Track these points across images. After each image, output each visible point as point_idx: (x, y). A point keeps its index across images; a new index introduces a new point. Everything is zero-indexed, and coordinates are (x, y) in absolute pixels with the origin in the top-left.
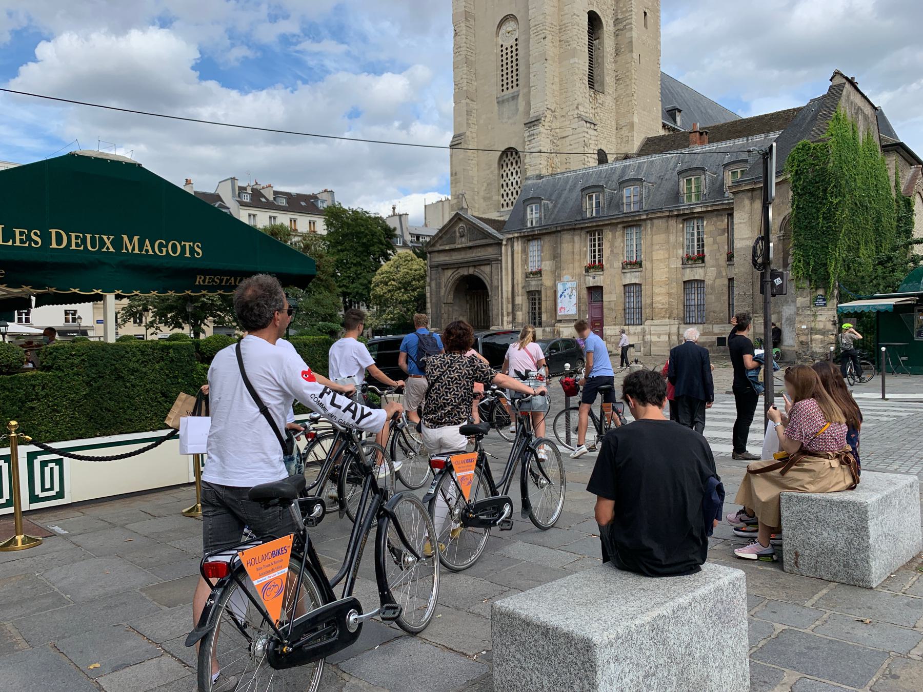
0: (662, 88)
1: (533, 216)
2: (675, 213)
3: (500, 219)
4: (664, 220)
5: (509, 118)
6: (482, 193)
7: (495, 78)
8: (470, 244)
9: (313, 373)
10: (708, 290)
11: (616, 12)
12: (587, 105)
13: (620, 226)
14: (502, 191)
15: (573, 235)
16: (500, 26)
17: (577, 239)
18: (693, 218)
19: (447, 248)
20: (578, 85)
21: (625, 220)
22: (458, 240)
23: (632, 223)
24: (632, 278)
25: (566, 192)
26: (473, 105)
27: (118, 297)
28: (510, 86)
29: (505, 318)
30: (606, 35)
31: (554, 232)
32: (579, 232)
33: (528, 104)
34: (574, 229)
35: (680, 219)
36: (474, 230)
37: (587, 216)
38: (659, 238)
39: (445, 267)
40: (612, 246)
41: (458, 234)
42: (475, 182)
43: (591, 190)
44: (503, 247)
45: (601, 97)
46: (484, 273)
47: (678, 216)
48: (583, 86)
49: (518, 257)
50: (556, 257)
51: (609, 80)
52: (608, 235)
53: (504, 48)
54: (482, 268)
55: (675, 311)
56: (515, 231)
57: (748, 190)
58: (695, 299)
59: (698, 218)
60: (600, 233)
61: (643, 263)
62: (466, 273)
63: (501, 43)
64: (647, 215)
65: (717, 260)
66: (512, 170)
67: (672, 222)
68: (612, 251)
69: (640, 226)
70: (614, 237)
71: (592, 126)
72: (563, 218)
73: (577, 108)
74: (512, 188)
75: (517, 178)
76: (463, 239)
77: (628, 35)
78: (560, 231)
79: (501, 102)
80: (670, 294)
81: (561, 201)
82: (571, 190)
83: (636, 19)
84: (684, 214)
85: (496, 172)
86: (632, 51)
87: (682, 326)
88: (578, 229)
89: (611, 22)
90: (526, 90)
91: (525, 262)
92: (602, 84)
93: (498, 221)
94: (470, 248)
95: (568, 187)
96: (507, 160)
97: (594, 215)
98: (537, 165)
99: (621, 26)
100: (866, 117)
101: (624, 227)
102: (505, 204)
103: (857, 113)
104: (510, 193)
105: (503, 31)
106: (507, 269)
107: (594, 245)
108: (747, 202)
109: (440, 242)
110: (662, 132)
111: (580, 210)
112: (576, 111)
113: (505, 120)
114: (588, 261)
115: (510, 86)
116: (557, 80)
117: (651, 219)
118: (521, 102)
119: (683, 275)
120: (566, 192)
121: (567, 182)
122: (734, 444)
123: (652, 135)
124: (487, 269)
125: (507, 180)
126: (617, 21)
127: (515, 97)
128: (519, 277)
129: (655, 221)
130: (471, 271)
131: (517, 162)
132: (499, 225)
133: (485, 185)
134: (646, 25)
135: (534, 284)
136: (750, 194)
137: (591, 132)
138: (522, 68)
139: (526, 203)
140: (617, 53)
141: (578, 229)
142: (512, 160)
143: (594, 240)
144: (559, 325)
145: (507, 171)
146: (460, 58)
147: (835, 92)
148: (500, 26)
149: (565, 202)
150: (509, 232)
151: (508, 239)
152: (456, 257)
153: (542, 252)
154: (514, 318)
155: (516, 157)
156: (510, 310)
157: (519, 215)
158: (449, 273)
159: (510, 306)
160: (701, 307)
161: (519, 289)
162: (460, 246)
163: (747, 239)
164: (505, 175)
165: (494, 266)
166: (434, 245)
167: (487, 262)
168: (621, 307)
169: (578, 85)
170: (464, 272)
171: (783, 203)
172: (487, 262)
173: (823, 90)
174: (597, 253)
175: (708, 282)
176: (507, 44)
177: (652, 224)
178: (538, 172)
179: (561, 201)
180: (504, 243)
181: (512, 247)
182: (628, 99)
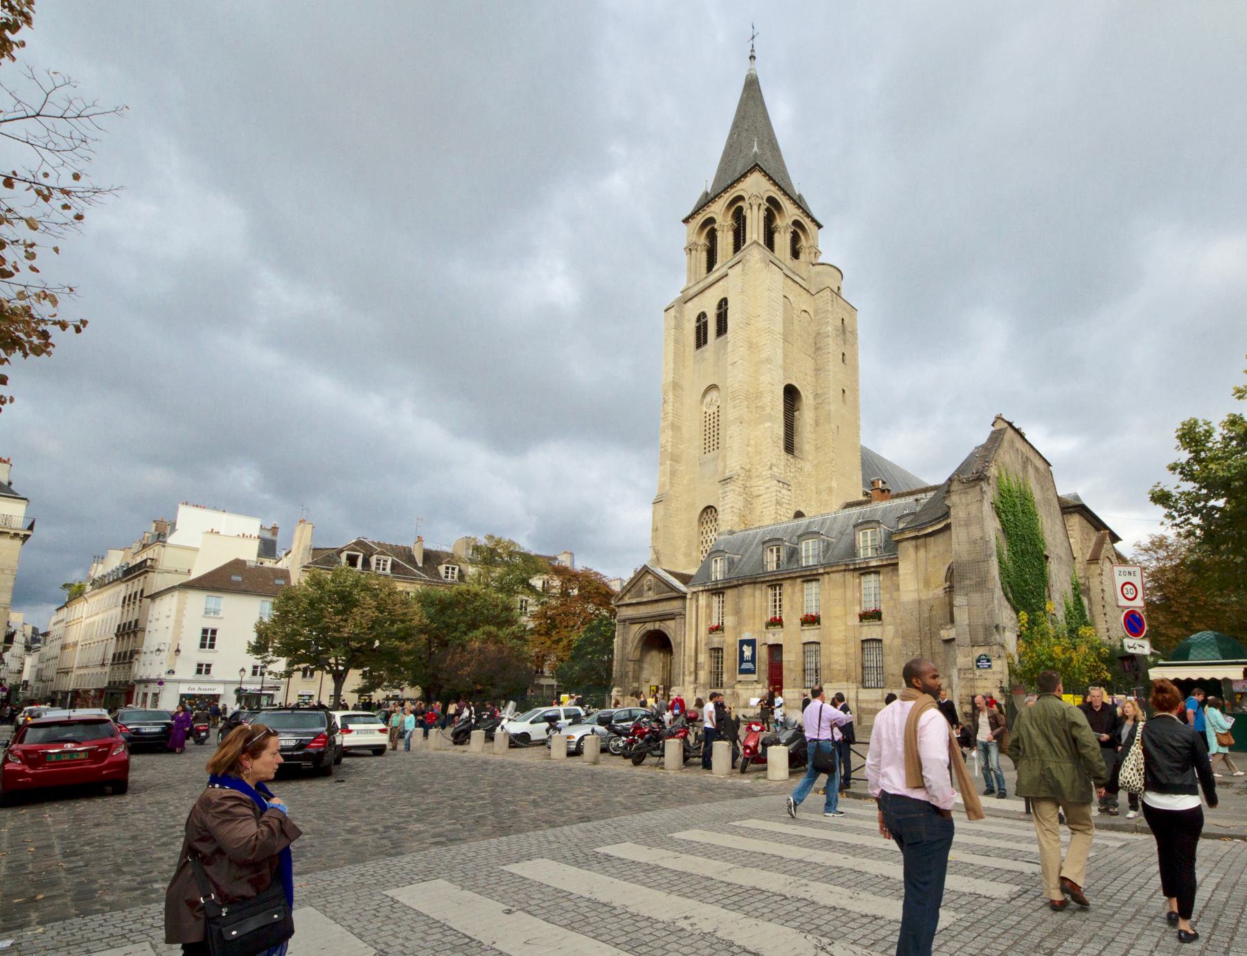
0: (862, 459)
1: (718, 570)
7: (699, 441)
8: (656, 597)
10: (886, 650)
13: (799, 580)
17: (758, 593)
18: (870, 573)
22: (645, 595)
23: (810, 577)
24: (810, 634)
27: (285, 574)
29: (687, 678)
31: (735, 586)
34: (755, 583)
35: (856, 574)
37: (771, 568)
38: (838, 593)
39: (634, 621)
40: (791, 601)
45: (801, 464)
46: (669, 628)
47: (855, 570)
49: (702, 612)
50: (737, 612)
52: (786, 584)
55: (853, 674)
56: (700, 585)
58: (872, 659)
60: (781, 585)
65: (894, 617)
67: (849, 576)
68: (791, 607)
72: (747, 570)
80: (847, 654)
81: (747, 555)
83: (833, 393)
84: (860, 569)
87: (861, 690)
89: (811, 397)
91: (710, 617)
92: (801, 451)
98: (727, 519)
99: (819, 400)
100: (1037, 469)
103: (1025, 468)
105: (708, 398)
111: (762, 564)
114: (770, 616)
117: (828, 573)
119: (861, 633)
121: (755, 538)
122: (946, 861)
124: (671, 623)
126: (816, 396)
128: (703, 630)
130: (657, 626)
132: (685, 579)
135: (716, 640)
136: (914, 542)
137: (784, 491)
140: (817, 424)
144: (738, 686)
147: (996, 438)
149: (751, 557)
150: (694, 586)
154: (696, 679)
156: (692, 669)
157: (705, 568)
158: (636, 628)
159: (693, 665)
160: (880, 669)
161: (703, 648)
167: (671, 617)
168: (800, 668)
170: (650, 626)
172: (671, 617)
173: (982, 438)
175: (885, 642)
176: (710, 411)
179: (747, 555)
180: (689, 596)
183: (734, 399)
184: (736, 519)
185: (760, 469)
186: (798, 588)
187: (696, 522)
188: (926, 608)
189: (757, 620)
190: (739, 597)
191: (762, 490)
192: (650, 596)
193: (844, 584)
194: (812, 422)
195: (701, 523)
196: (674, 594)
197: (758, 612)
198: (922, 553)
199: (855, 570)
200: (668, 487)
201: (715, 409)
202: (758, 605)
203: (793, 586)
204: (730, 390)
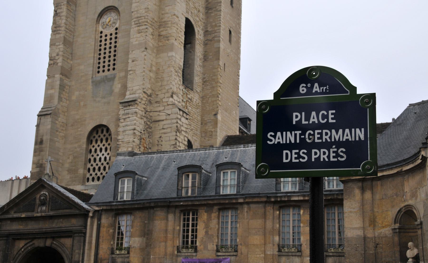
2: (273, 200)
3: (85, 192)
4: (261, 205)
5: (104, 98)
6: (67, 166)
8: (51, 213)
9: (123, 249)
11: (206, 26)
12: (180, 96)
13: (216, 208)
14: (89, 166)
15: (168, 213)
16: (101, 15)
17: (171, 217)
18: (289, 206)
19: (23, 216)
20: (174, 77)
21: (222, 202)
23: (227, 205)
25: (160, 170)
26: (66, 81)
28: (106, 68)
30: (197, 42)
32: (173, 209)
33: (125, 87)
35: (277, 207)
36: (58, 200)
38: (257, 223)
40: (207, 227)
41: (38, 202)
42: (61, 154)
43: (187, 170)
44: (89, 220)
45: (191, 95)
47: (275, 202)
48: (178, 78)
51: (197, 80)
52: (203, 216)
53: (103, 35)
54: (63, 240)
57: (359, 180)
59: (294, 207)
61: (239, 247)
62: (42, 245)
63: (101, 29)
64: (245, 199)
66: (101, 146)
67: (269, 209)
68: (207, 232)
69: (236, 209)
70: (209, 219)
71: (185, 115)
73: (172, 97)
74: (100, 164)
75: (106, 154)
76: (44, 208)
77: (216, 45)
78: (153, 208)
79: (96, 84)
82: (164, 169)
83: (223, 34)
84: (281, 202)
85: (85, 146)
86: (218, 59)
88: (173, 206)
89: (201, 32)
90: (122, 74)
93: (83, 193)
94: (51, 217)
95: (162, 166)
96: (97, 137)
97: (190, 194)
101: (220, 210)
102: (91, 178)
104: (97, 168)
105: (106, 19)
106: (90, 243)
107: (188, 225)
108: (357, 192)
109: (15, 209)
110: (238, 133)
112: (171, 99)
113: (98, 99)
115: (106, 68)
116: (154, 68)
117: (248, 203)
118: (117, 87)
120: (160, 170)
123: (231, 133)
124: (68, 242)
125: (95, 155)
126: (206, 33)
127: (112, 79)
129: (252, 206)
130: (48, 243)
131: (107, 140)
133: (71, 157)
134: (230, 41)
137: (183, 120)
138: (119, 54)
139: (119, 176)
140: (205, 58)
141: (173, 206)
142: (102, 136)
143: (188, 220)
145: (96, 146)
146: (58, 36)
148: (101, 15)
151: (95, 211)
152: (32, 227)
153: (132, 226)
155: (107, 135)
158: (21, 244)
162: (39, 215)
163: (358, 228)
164: (93, 150)
165: (77, 239)
166: (7, 212)
167: (68, 234)
169: (174, 77)
170: (39, 243)
171: (397, 195)
172: (68, 234)
174: (190, 234)
176: (107, 32)
177: (249, 209)
178: (130, 149)
180: (91, 214)
181: (99, 220)
182: (214, 99)
183: (139, 25)
184: (137, 141)
185: (161, 96)
186: (214, 215)
187: (85, 140)
188: (371, 245)
189: (169, 243)
190: (151, 219)
191: (163, 116)
192: (42, 211)
193: (264, 216)
194: (202, 57)
195: (90, 141)
196: (77, 212)
197: (170, 236)
198: (368, 195)
199: (275, 202)
200: (56, 101)
201: (113, 31)
202: (170, 228)
203: (209, 212)
204: (135, 15)
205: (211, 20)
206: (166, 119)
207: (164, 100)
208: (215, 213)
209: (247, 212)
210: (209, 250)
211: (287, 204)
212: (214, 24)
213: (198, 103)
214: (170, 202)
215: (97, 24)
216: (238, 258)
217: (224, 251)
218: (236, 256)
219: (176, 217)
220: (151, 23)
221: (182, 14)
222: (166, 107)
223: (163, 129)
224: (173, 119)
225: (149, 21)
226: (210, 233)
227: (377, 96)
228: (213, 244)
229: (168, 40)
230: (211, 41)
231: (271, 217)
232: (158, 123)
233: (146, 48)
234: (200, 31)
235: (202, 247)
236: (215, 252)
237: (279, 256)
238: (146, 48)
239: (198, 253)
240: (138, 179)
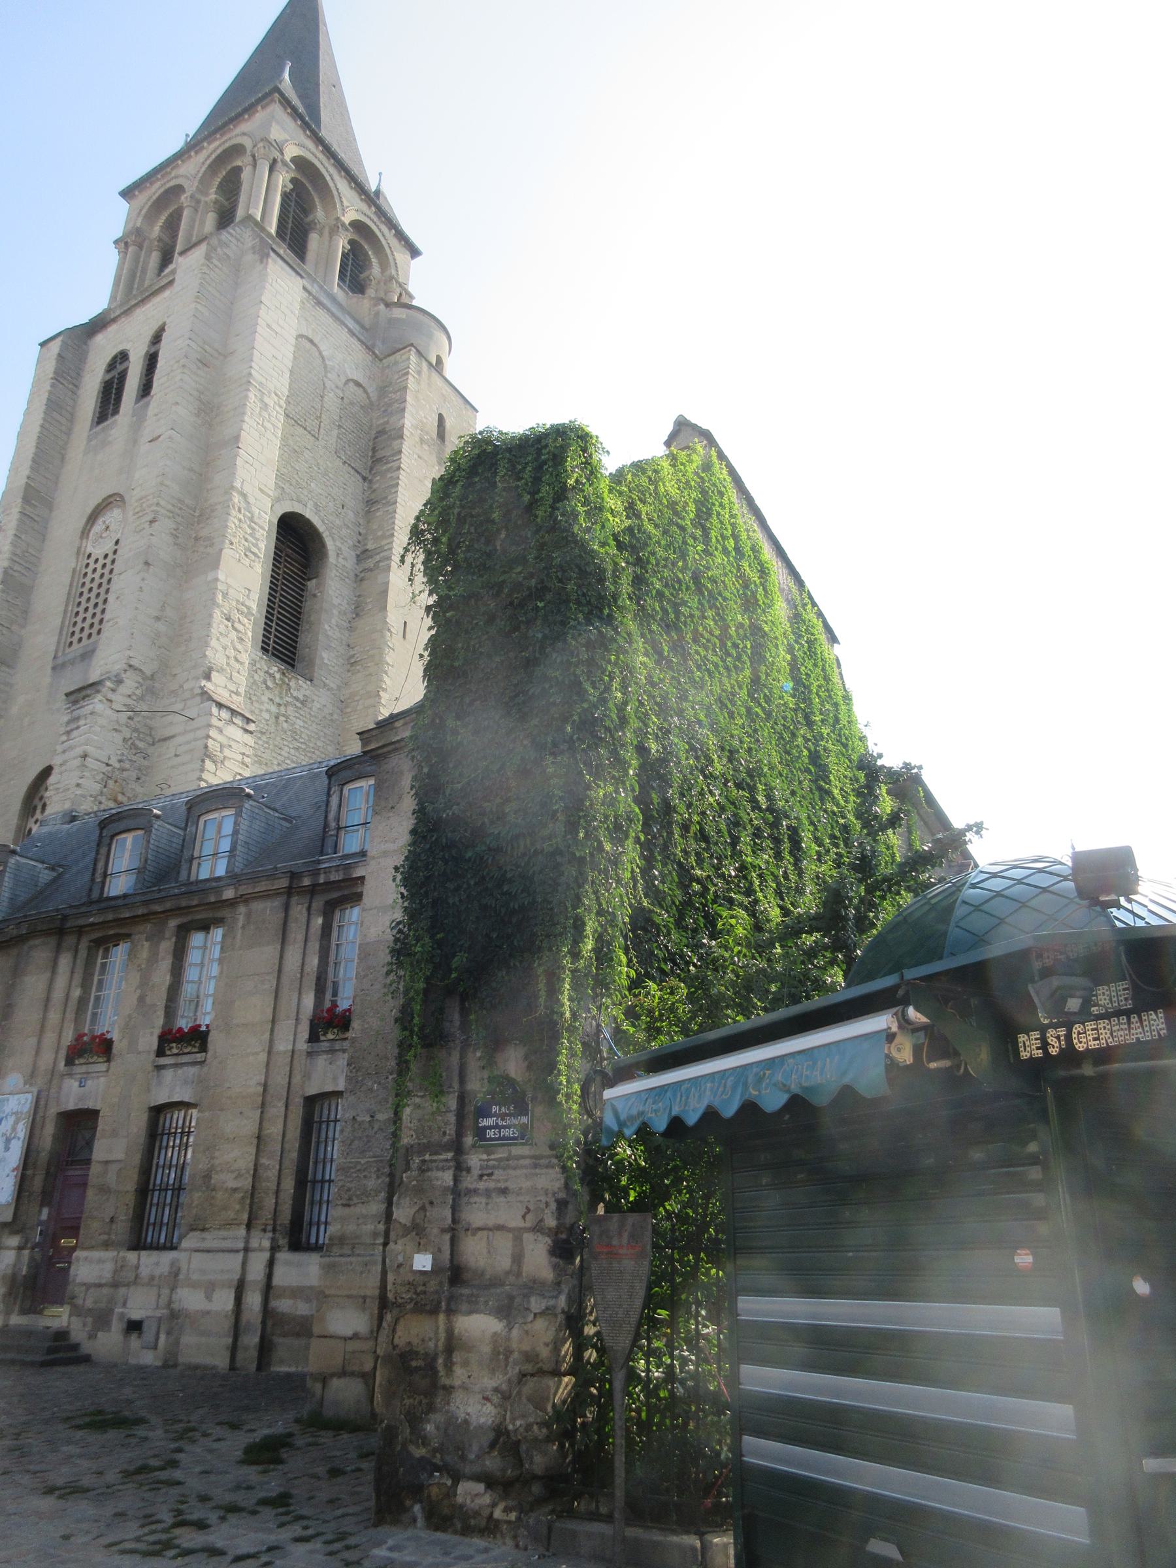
89: (350, 555)
148: (93, 517)
205: (375, 527)
206: (185, 732)
207: (186, 686)
208: (170, 939)
209: (243, 927)
210: (139, 1053)
211: (346, 892)
212: (380, 533)
213: (331, 714)
214: (65, 918)
215: (81, 538)
216: (205, 1069)
217: (175, 1051)
218: (202, 1063)
219: (78, 961)
220: (170, 507)
221: (260, 489)
222: (189, 703)
223: (176, 755)
224: (198, 729)
225: (162, 503)
226: (148, 1000)
227: (121, 189)
228: (152, 1034)
229: (212, 545)
230: (371, 570)
231: (300, 937)
232: (167, 743)
233: (147, 563)
234: (345, 549)
235: (125, 1043)
236: (152, 1055)
237: (309, 1054)
238: (147, 563)
239: (113, 1063)
240: (18, 866)
